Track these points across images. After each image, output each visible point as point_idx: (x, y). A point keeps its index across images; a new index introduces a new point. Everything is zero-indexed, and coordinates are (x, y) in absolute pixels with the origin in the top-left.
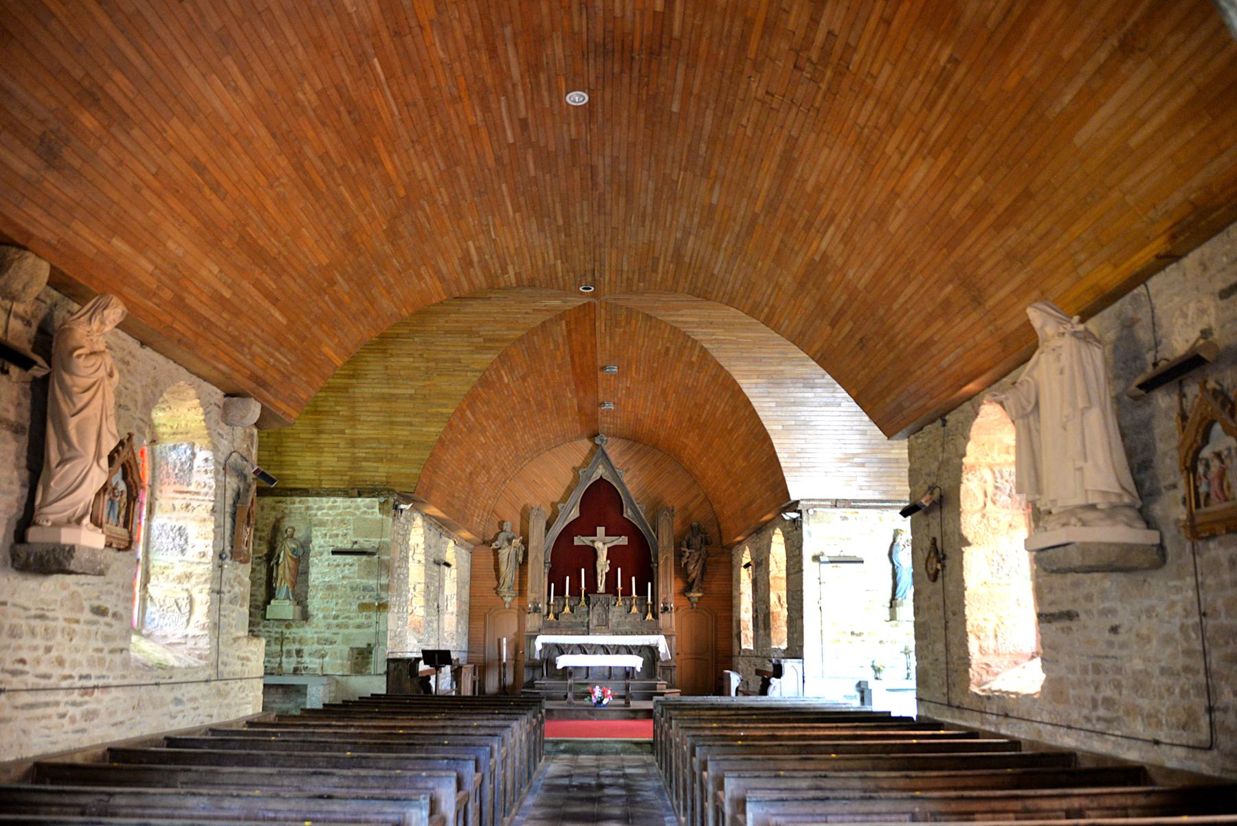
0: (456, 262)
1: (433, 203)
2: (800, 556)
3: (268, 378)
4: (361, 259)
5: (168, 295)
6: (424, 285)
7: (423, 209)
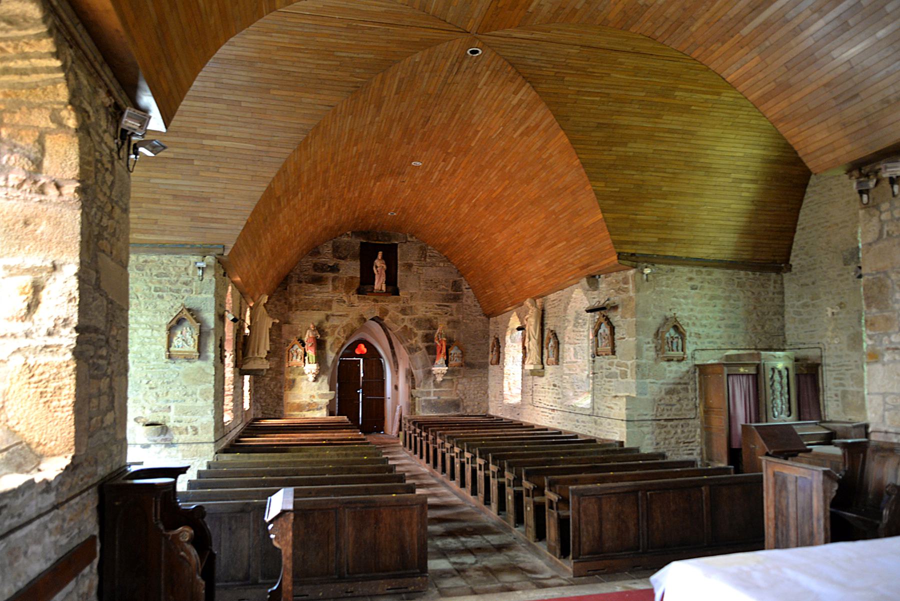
0: (532, 137)
1: (505, 166)
2: (472, 486)
3: (586, 262)
4: (543, 196)
5: (543, 279)
6: (555, 153)
7: (510, 169)
